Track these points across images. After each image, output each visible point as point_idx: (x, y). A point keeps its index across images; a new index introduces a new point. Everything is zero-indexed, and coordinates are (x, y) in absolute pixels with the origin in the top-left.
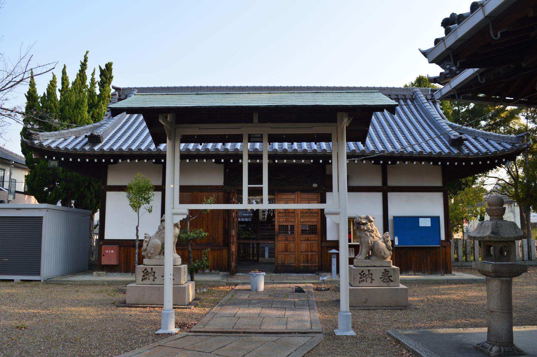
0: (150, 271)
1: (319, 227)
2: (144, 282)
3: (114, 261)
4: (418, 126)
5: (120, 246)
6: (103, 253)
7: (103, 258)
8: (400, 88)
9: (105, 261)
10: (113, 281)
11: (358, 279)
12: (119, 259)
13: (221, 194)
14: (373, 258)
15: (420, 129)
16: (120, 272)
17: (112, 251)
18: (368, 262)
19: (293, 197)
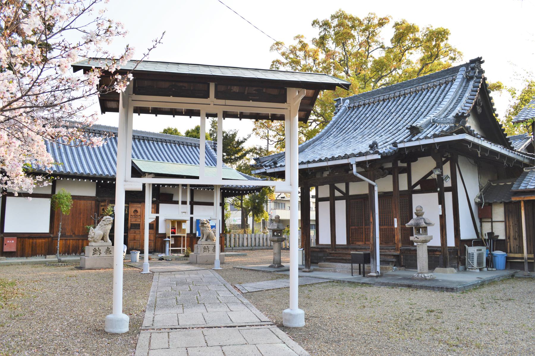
0: (97, 249)
1: (155, 225)
2: (94, 256)
3: (13, 249)
4: (189, 159)
5: (18, 238)
6: (5, 243)
7: (5, 246)
8: (353, 182)
9: (6, 249)
10: (25, 262)
11: (203, 251)
12: (17, 248)
13: (93, 202)
14: (209, 240)
15: (142, 151)
16: (17, 257)
17: (13, 241)
18: (207, 243)
19: (140, 205)
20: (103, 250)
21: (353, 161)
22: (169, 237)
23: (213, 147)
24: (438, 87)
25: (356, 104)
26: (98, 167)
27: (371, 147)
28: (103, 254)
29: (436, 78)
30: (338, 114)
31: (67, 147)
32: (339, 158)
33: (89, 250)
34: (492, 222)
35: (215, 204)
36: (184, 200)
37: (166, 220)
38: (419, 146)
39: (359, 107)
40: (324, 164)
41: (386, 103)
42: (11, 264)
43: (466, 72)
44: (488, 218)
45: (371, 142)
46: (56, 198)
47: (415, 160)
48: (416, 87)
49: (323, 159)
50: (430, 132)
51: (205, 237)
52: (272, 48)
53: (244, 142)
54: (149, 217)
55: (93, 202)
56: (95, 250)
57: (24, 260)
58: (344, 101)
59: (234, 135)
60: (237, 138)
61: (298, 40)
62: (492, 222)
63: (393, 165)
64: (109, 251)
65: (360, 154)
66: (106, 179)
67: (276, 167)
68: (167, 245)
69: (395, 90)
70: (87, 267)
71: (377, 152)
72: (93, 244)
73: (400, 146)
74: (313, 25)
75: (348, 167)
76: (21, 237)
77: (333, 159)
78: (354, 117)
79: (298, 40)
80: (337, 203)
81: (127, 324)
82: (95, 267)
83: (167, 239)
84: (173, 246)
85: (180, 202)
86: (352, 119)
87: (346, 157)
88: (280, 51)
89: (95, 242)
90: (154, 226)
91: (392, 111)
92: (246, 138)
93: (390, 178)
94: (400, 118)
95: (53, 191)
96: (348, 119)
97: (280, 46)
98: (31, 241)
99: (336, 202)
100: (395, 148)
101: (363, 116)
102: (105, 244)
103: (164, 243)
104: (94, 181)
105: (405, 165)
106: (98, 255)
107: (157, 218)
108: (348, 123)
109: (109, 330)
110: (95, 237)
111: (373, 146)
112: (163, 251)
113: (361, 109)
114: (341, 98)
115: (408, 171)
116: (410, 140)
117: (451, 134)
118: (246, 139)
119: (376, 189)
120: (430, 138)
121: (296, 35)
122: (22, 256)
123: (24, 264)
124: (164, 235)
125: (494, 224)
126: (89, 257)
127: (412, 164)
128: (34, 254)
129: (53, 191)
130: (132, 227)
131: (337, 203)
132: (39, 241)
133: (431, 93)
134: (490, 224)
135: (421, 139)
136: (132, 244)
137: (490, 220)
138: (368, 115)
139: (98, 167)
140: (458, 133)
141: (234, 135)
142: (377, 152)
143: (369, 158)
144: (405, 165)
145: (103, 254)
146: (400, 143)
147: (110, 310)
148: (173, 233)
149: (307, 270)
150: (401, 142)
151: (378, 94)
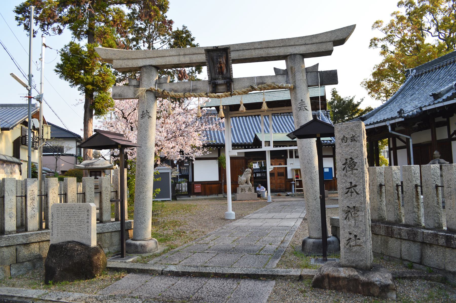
3: (200, 191)
9: (196, 191)
13: (244, 160)
20: (247, 189)
21: (388, 123)
22: (294, 181)
23: (326, 115)
25: (420, 73)
26: (244, 138)
27: (399, 112)
28: (247, 192)
30: (406, 83)
31: (212, 131)
32: (381, 122)
37: (292, 170)
38: (435, 108)
39: (422, 75)
40: (376, 125)
42: (199, 199)
46: (221, 159)
47: (452, 115)
49: (372, 123)
52: (373, 27)
53: (359, 105)
55: (244, 160)
56: (242, 190)
57: (206, 197)
58: (412, 70)
59: (351, 100)
60: (355, 102)
61: (395, 16)
65: (392, 118)
68: (293, 186)
70: (238, 199)
72: (241, 186)
73: (424, 109)
74: (398, 6)
75: (386, 127)
76: (203, 184)
77: (377, 122)
79: (395, 16)
80: (399, 151)
81: (234, 216)
82: (242, 199)
83: (293, 182)
84: (297, 187)
87: (384, 121)
88: (380, 28)
89: (242, 184)
92: (359, 101)
93: (429, 131)
95: (219, 155)
97: (380, 24)
98: (209, 186)
102: (248, 185)
103: (291, 185)
105: (445, 119)
109: (226, 218)
111: (400, 112)
112: (291, 191)
113: (423, 76)
114: (410, 69)
115: (447, 124)
116: (434, 104)
118: (360, 103)
119: (411, 140)
120: (441, 102)
121: (392, 12)
122: (205, 195)
123: (205, 199)
124: (292, 180)
127: (451, 118)
128: (211, 194)
129: (219, 155)
131: (399, 151)
132: (214, 186)
139: (244, 138)
141: (351, 100)
143: (397, 120)
144: (445, 119)
145: (247, 192)
146: (424, 107)
147: (227, 210)
148: (297, 178)
150: (425, 106)
151: (436, 63)
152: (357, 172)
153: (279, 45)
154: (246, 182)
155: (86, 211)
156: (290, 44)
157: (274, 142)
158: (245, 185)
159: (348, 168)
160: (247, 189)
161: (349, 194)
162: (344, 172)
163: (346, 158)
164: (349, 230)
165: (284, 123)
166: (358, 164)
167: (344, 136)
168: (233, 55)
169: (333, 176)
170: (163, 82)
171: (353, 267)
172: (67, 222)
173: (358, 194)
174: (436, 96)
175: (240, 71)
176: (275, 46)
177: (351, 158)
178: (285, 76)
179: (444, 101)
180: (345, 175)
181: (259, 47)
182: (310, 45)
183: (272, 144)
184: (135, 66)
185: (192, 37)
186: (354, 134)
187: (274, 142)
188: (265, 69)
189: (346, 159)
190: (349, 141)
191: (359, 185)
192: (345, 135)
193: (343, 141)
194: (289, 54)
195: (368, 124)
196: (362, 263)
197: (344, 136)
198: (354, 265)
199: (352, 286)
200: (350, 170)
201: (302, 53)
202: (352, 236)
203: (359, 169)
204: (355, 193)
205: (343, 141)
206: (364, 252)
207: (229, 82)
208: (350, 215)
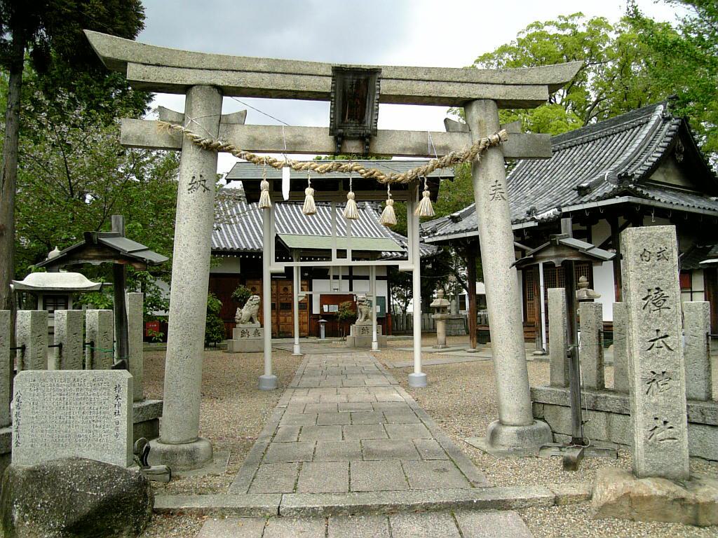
20: (252, 332)
24: (631, 130)
28: (252, 337)
29: (630, 120)
33: (236, 332)
34: (692, 292)
35: (370, 278)
36: (336, 274)
38: (583, 210)
40: (451, 237)
41: (572, 151)
43: (663, 112)
44: (687, 288)
45: (528, 209)
47: (596, 222)
48: (606, 131)
50: (598, 192)
51: (363, 317)
54: (298, 295)
56: (243, 332)
62: (692, 292)
63: (587, 228)
64: (257, 333)
66: (251, 253)
67: (434, 236)
69: (583, 134)
70: (236, 350)
71: (533, 219)
72: (241, 325)
78: (535, 169)
85: (340, 277)
86: (532, 173)
90: (306, 305)
91: (575, 163)
94: (580, 173)
96: (527, 173)
99: (348, 281)
100: (559, 212)
101: (544, 169)
104: (238, 256)
105: (585, 228)
106: (246, 338)
107: (311, 296)
108: (527, 178)
110: (243, 318)
117: (605, 199)
120: (593, 201)
125: (693, 294)
126: (237, 340)
130: (282, 305)
133: (622, 139)
134: (690, 294)
135: (586, 203)
136: (282, 332)
137: (690, 290)
138: (549, 168)
140: (621, 195)
142: (533, 219)
144: (585, 228)
145: (252, 337)
146: (565, 206)
149: (473, 350)
152: (669, 313)
153: (461, 79)
154: (251, 320)
155: (112, 389)
156: (479, 80)
157: (353, 251)
158: (249, 324)
159: (652, 306)
160: (252, 332)
161: (654, 350)
162: (646, 312)
163: (649, 287)
164: (653, 413)
165: (320, 221)
166: (670, 299)
167: (645, 250)
168: (385, 87)
169: (387, 312)
170: (234, 122)
171: (660, 476)
172: (60, 413)
173: (669, 349)
174: (582, 191)
175: (389, 117)
176: (454, 80)
177: (658, 289)
178: (467, 136)
179: (599, 199)
180: (647, 318)
181: (426, 77)
182: (512, 86)
183: (349, 254)
184: (179, 83)
185: (649, 22)
186: (663, 248)
187: (353, 251)
188: (430, 120)
189: (649, 290)
190: (654, 258)
191: (672, 334)
192: (647, 249)
193: (644, 258)
194: (476, 97)
195: (453, 232)
196: (676, 468)
197: (645, 250)
198: (662, 472)
199: (662, 510)
200: (656, 308)
201: (495, 98)
202: (659, 423)
203: (672, 307)
204: (665, 348)
205: (644, 258)
206: (680, 449)
207: (368, 138)
208: (655, 387)
